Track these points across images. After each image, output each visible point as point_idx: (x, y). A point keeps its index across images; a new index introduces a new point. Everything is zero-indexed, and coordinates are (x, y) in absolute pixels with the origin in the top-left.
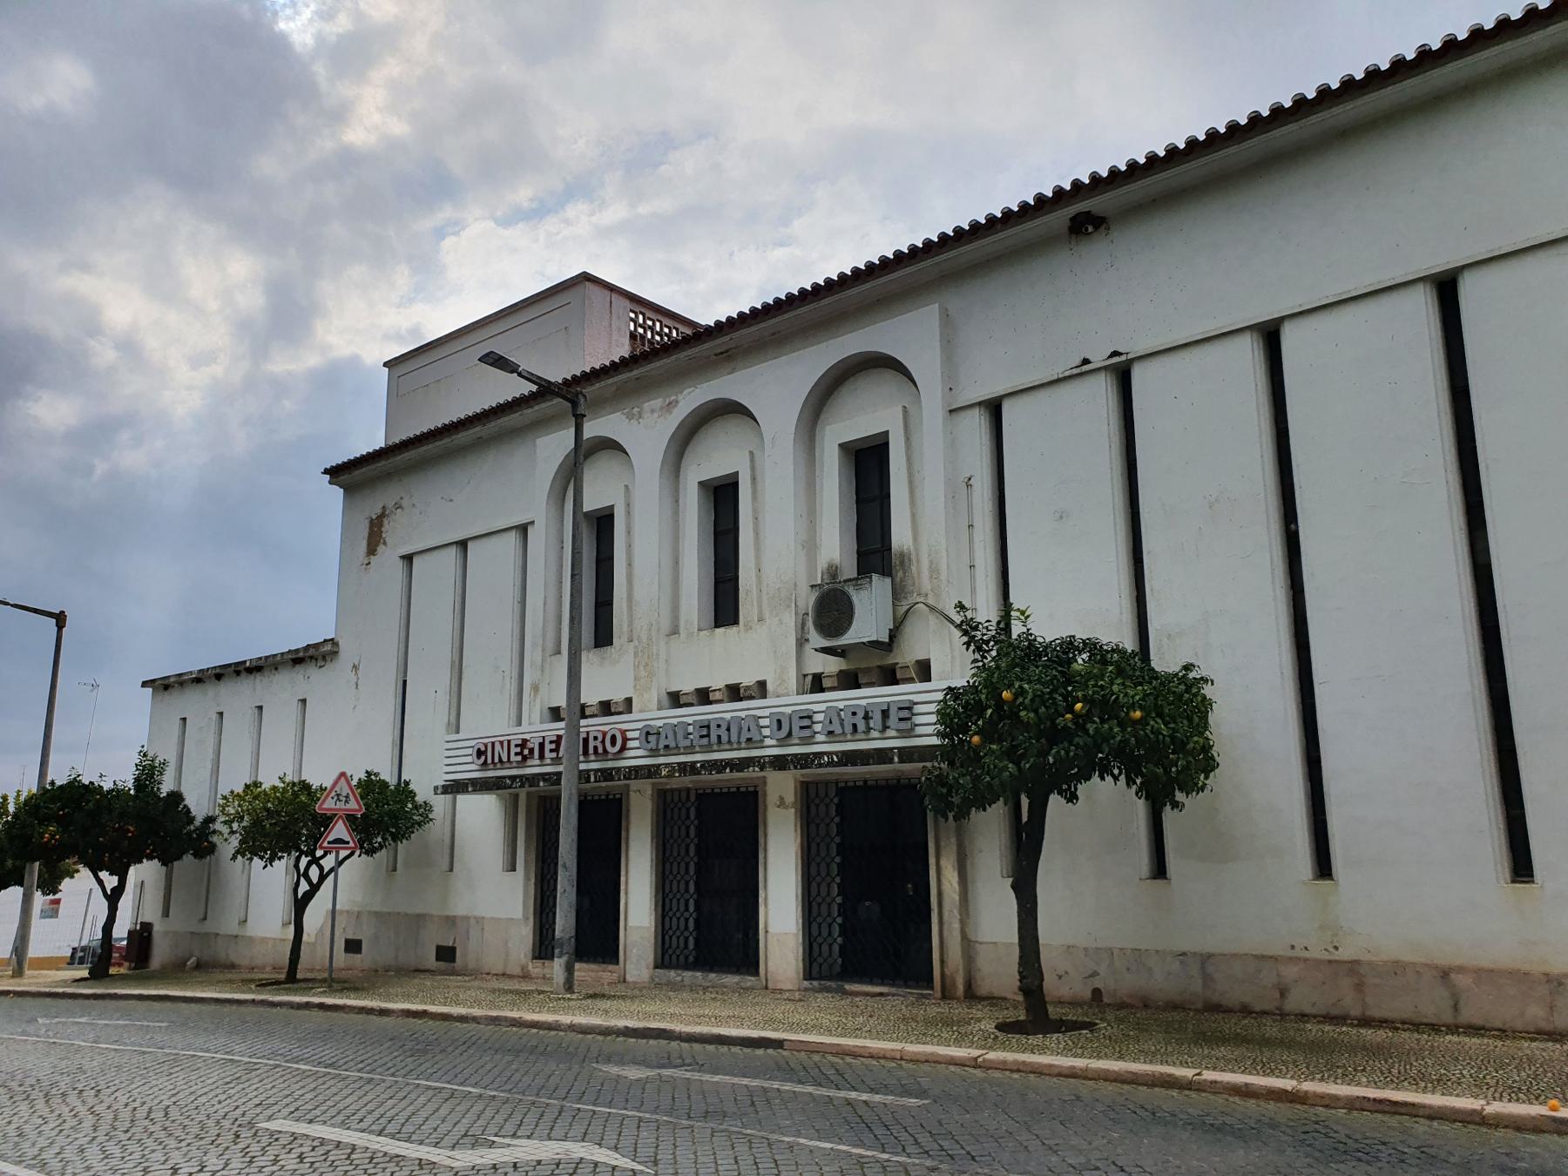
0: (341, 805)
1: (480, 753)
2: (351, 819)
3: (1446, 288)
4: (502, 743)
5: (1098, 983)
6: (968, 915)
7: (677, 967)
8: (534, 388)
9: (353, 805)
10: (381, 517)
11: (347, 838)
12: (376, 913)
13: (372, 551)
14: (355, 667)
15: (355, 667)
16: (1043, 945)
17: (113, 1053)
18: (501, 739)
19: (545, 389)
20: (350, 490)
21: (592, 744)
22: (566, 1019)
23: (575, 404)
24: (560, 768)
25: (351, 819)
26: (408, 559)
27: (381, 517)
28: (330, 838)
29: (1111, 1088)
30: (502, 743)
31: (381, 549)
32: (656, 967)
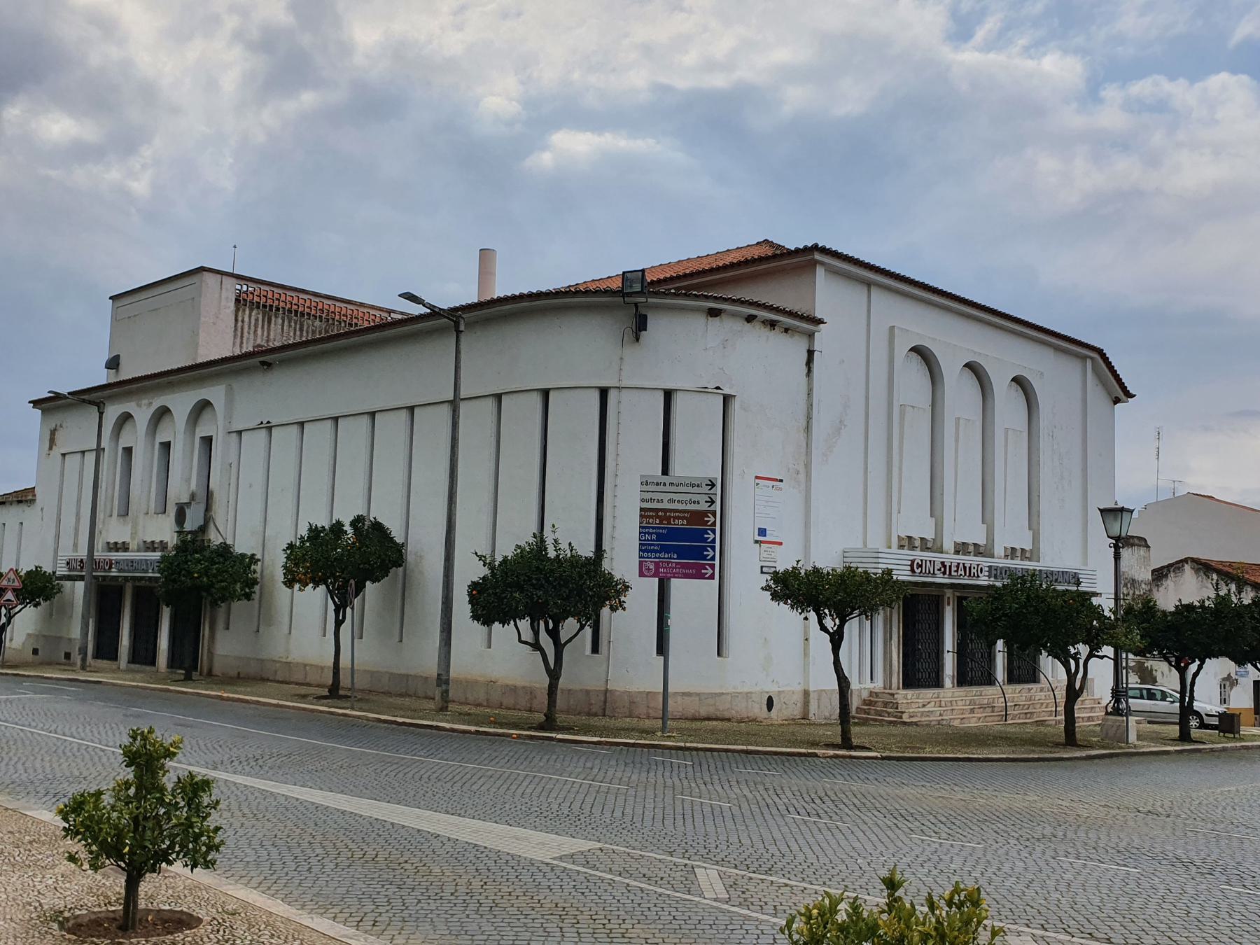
0: (10, 584)
1: (68, 563)
2: (14, 590)
3: (604, 392)
4: (930, 561)
5: (240, 670)
6: (213, 643)
7: (139, 663)
8: (429, 311)
9: (16, 584)
10: (55, 430)
11: (13, 599)
12: (44, 636)
13: (51, 448)
14: (42, 509)
15: (42, 509)
16: (343, 669)
17: (19, 722)
18: (921, 558)
19: (435, 313)
20: (44, 411)
21: (973, 571)
22: (55, 676)
23: (457, 324)
24: (84, 573)
25: (14, 590)
26: (64, 455)
27: (55, 430)
28: (5, 599)
29: (328, 716)
30: (930, 561)
31: (54, 447)
32: (129, 662)
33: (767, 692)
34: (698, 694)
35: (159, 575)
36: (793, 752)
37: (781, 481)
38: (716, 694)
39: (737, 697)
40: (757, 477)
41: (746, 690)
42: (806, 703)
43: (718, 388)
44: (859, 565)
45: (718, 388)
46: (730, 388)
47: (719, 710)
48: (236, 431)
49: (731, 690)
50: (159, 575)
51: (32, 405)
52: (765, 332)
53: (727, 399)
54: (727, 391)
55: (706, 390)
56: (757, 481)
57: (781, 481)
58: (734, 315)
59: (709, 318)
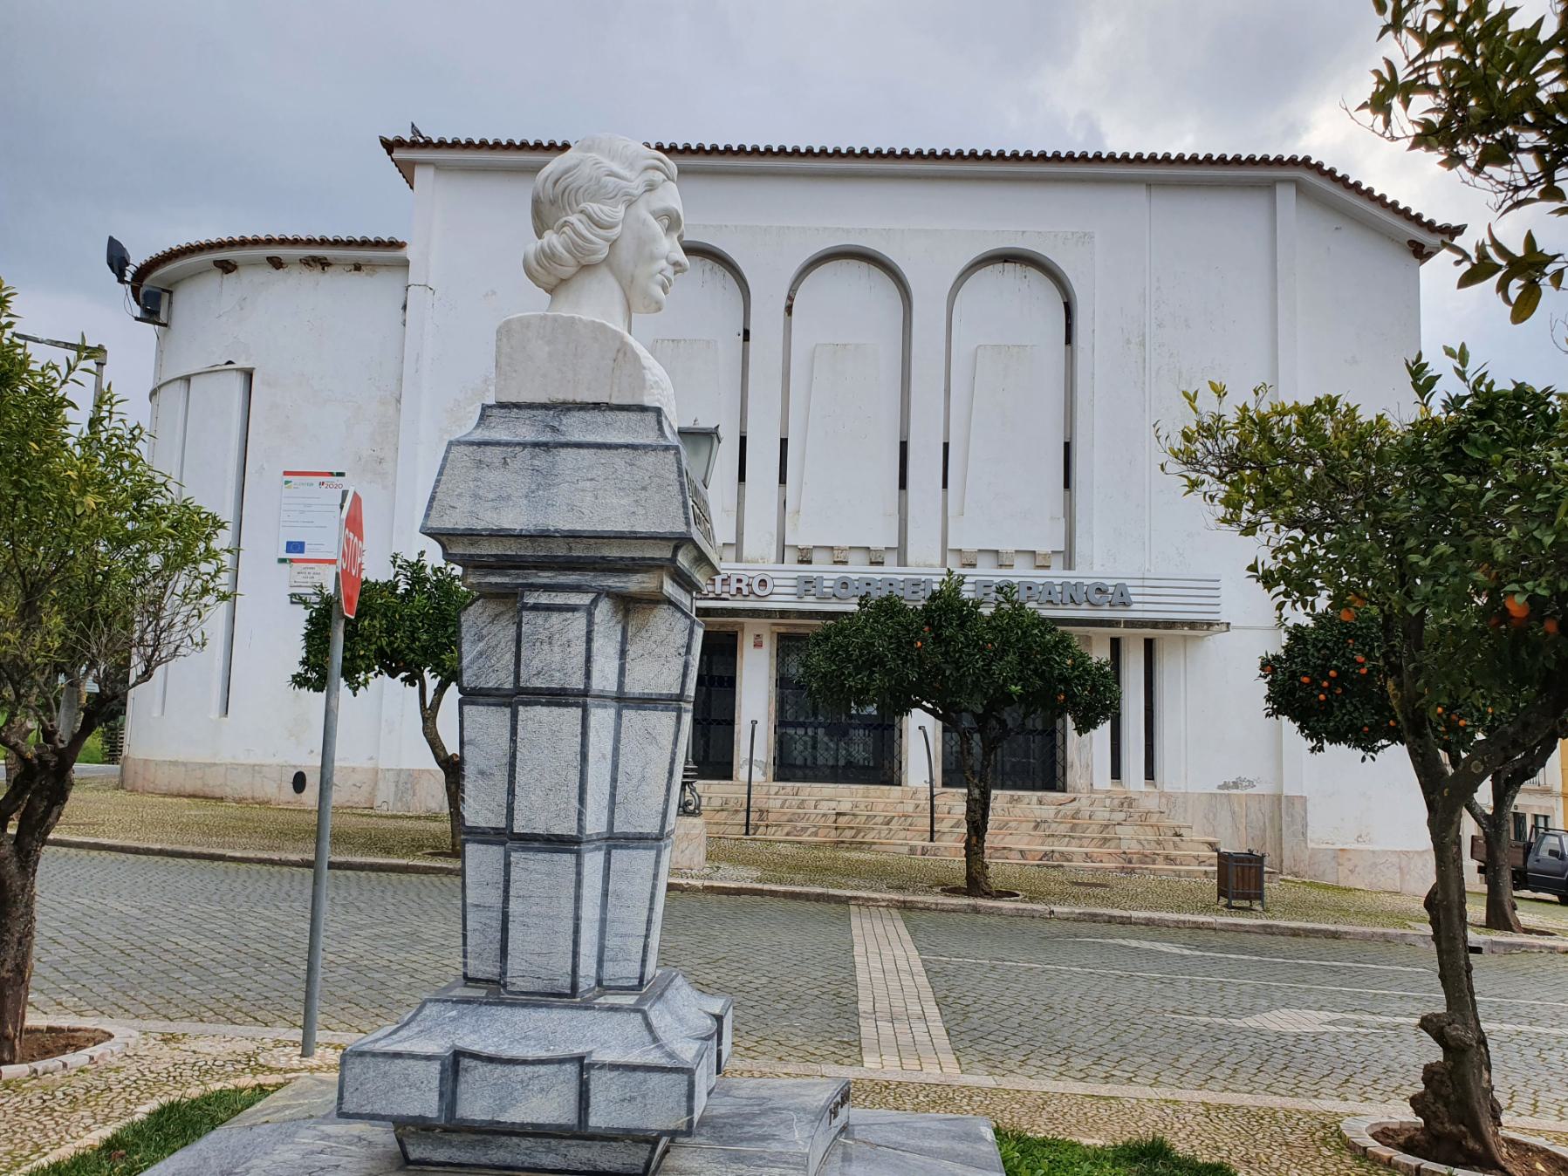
33: (295, 767)
34: (185, 764)
35: (1446, 476)
36: (381, 865)
37: (341, 474)
38: (205, 764)
39: (236, 769)
40: (286, 473)
41: (252, 761)
42: (375, 787)
43: (230, 363)
44: (825, 576)
45: (230, 363)
46: (246, 360)
47: (208, 785)
48: (181, 378)
49: (228, 760)
50: (1446, 476)
51: (1390, 34)
52: (313, 276)
53: (249, 374)
54: (241, 363)
55: (217, 368)
56: (288, 478)
57: (341, 474)
58: (253, 264)
59: (225, 276)
